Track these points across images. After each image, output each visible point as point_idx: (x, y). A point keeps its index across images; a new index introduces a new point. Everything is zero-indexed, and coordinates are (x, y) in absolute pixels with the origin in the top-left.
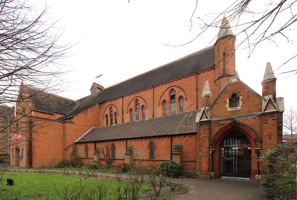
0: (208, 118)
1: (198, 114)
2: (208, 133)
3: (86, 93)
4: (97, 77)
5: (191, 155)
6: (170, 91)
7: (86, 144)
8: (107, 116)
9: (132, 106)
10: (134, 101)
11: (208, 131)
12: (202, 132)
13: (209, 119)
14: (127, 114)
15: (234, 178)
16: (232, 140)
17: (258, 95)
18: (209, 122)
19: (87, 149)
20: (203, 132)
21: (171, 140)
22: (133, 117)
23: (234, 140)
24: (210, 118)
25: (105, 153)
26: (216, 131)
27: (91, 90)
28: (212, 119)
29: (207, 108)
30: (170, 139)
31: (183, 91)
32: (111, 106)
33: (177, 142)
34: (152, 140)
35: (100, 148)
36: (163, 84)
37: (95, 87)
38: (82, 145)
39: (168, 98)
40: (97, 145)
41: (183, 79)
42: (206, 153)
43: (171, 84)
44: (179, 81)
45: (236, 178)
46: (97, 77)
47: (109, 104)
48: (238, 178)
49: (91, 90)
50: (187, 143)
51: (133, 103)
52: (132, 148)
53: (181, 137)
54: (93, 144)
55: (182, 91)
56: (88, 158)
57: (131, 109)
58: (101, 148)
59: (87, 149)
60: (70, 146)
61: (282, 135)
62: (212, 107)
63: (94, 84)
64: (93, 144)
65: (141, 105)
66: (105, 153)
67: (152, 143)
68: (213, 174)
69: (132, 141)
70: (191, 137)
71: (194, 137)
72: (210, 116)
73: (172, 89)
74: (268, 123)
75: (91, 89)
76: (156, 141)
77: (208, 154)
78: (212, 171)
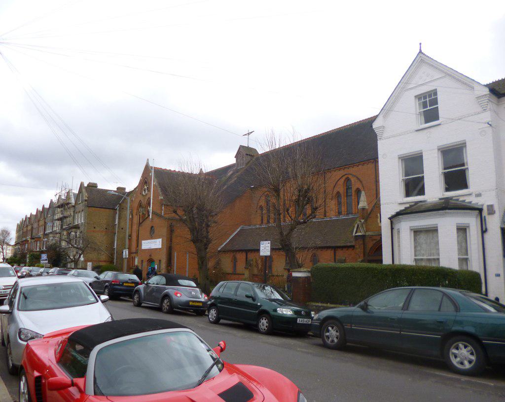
3: (235, 159)
4: (251, 133)
6: (345, 181)
7: (234, 253)
8: (261, 208)
9: (341, 189)
10: (342, 180)
11: (362, 246)
18: (363, 237)
19: (235, 261)
20: (358, 247)
21: (335, 253)
24: (365, 232)
25: (260, 266)
26: (370, 247)
27: (235, 157)
28: (367, 234)
30: (333, 252)
31: (361, 182)
32: (348, 177)
35: (252, 260)
36: (345, 168)
37: (245, 153)
39: (342, 189)
40: (248, 255)
41: (360, 167)
43: (346, 171)
44: (355, 169)
46: (251, 133)
47: (345, 174)
49: (235, 157)
53: (345, 250)
55: (359, 182)
56: (237, 273)
58: (254, 260)
59: (235, 261)
61: (311, 324)
63: (241, 147)
64: (244, 254)
65: (354, 189)
66: (260, 266)
67: (315, 256)
73: (348, 177)
75: (236, 155)
76: (319, 252)
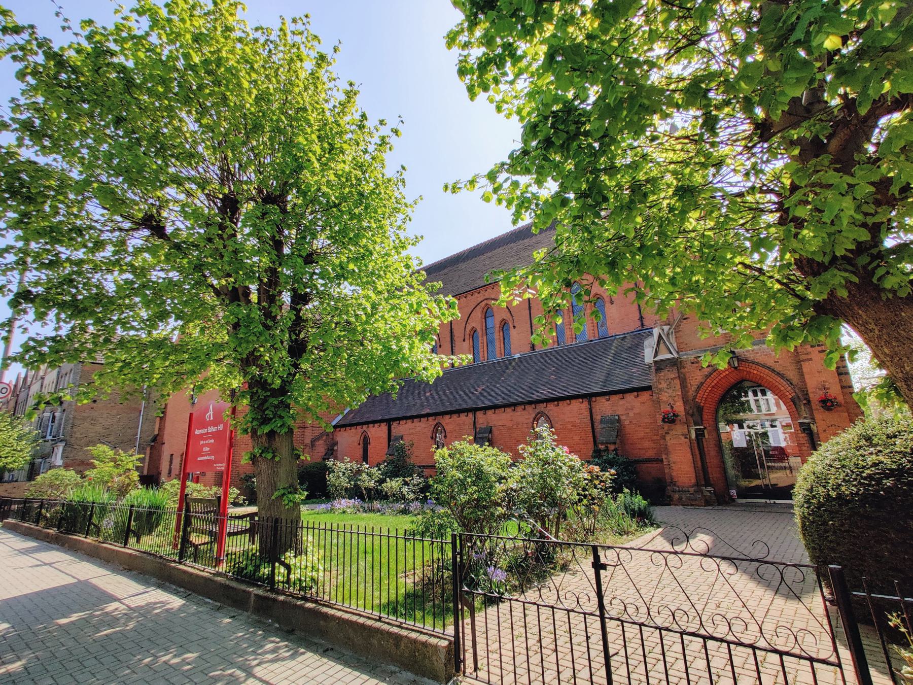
0: (671, 353)
1: (646, 343)
2: (678, 387)
5: (647, 444)
12: (664, 385)
13: (676, 355)
14: (464, 343)
15: (768, 501)
16: (755, 394)
17: (184, 605)
22: (481, 350)
23: (759, 394)
24: (678, 353)
29: (666, 328)
33: (604, 407)
34: (439, 419)
38: (353, 430)
42: (683, 438)
45: (772, 501)
48: (777, 501)
50: (631, 414)
51: (478, 314)
52: (491, 432)
54: (384, 427)
57: (474, 331)
60: (6, 482)
62: (678, 325)
68: (710, 491)
69: (490, 412)
70: (639, 399)
71: (645, 395)
72: (675, 345)
74: (811, 359)
77: (687, 440)
78: (706, 485)
